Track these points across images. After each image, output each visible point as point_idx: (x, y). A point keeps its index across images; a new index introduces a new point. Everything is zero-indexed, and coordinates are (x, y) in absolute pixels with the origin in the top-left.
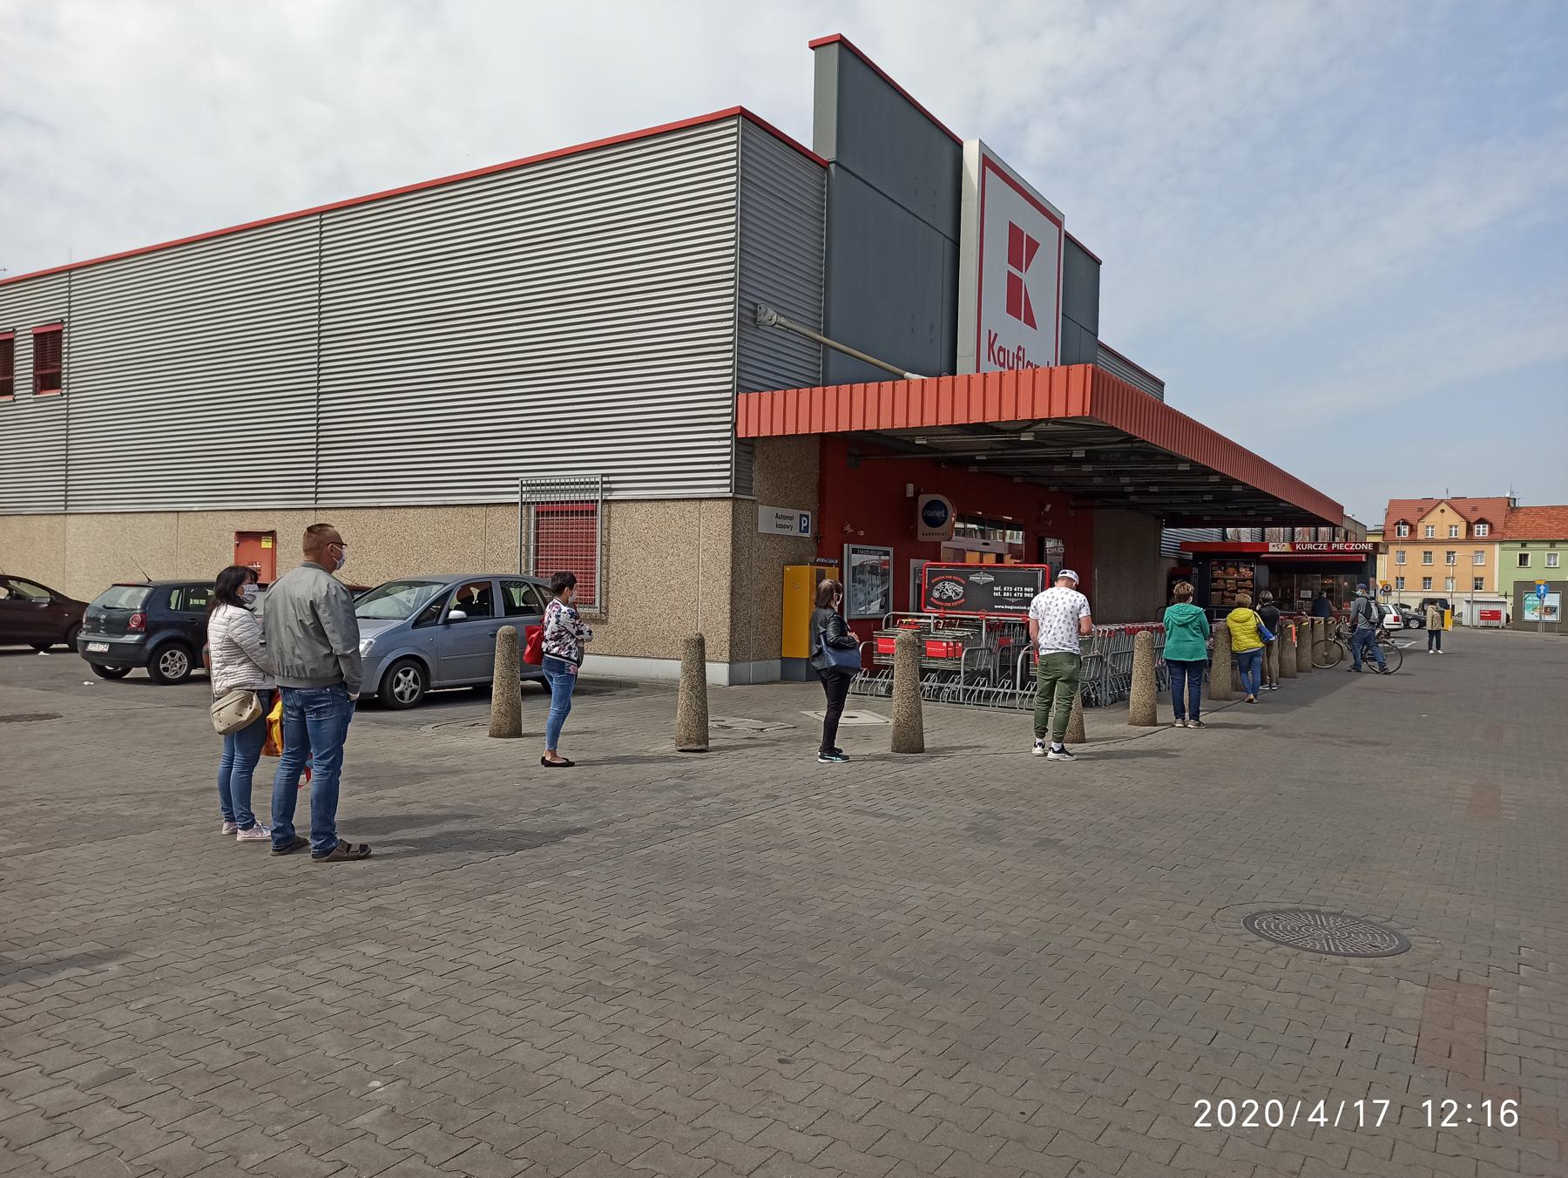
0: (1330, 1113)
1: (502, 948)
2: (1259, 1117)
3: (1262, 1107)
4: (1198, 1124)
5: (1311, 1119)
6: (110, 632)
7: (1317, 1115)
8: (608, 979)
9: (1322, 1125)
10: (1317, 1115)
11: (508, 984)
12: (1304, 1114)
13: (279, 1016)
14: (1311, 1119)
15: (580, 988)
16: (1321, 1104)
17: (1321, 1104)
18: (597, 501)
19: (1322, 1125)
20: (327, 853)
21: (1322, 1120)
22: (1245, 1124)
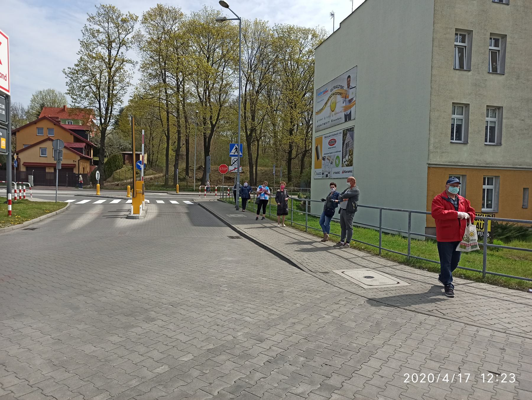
0: (450, 378)
1: (203, 317)
2: (426, 379)
3: (427, 376)
4: (405, 382)
5: (443, 380)
6: (108, 80)
7: (446, 379)
8: (170, 308)
9: (447, 382)
10: (446, 379)
11: (201, 307)
12: (441, 378)
13: (301, 55)
14: (443, 380)
15: (180, 305)
16: (447, 375)
17: (447, 375)
18: (310, 199)
19: (447, 382)
20: (309, 197)
21: (447, 380)
22: (421, 382)
